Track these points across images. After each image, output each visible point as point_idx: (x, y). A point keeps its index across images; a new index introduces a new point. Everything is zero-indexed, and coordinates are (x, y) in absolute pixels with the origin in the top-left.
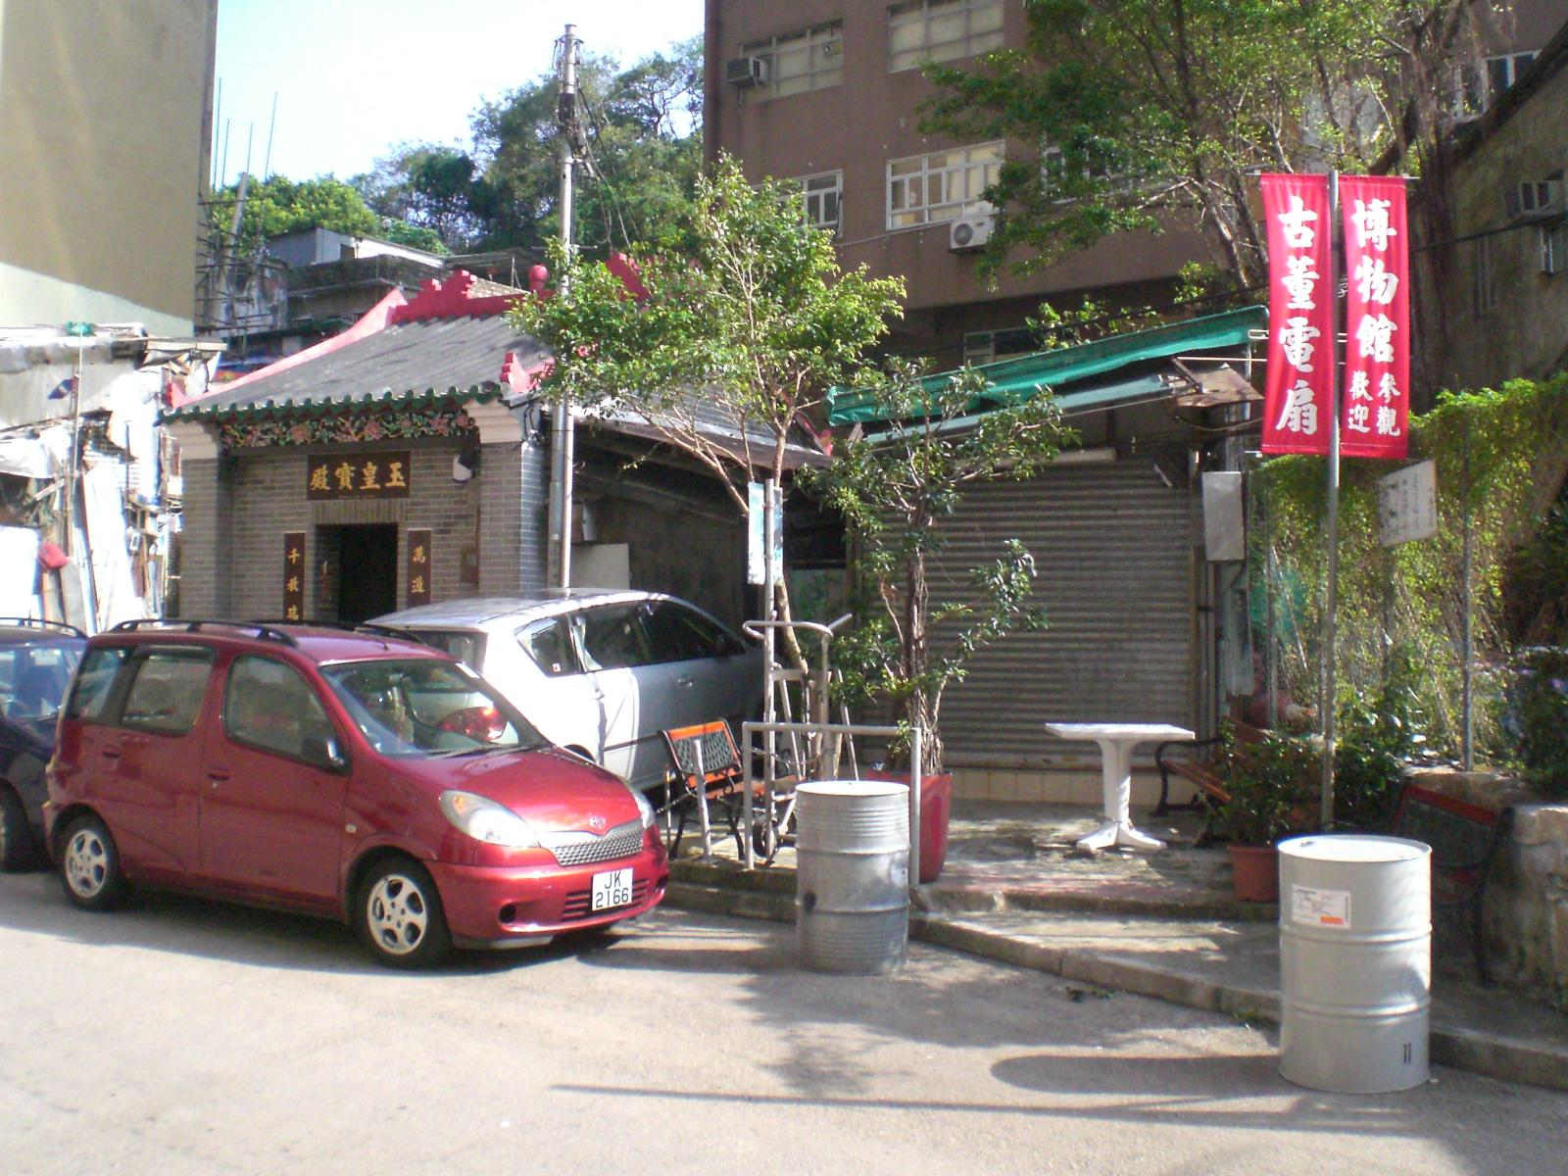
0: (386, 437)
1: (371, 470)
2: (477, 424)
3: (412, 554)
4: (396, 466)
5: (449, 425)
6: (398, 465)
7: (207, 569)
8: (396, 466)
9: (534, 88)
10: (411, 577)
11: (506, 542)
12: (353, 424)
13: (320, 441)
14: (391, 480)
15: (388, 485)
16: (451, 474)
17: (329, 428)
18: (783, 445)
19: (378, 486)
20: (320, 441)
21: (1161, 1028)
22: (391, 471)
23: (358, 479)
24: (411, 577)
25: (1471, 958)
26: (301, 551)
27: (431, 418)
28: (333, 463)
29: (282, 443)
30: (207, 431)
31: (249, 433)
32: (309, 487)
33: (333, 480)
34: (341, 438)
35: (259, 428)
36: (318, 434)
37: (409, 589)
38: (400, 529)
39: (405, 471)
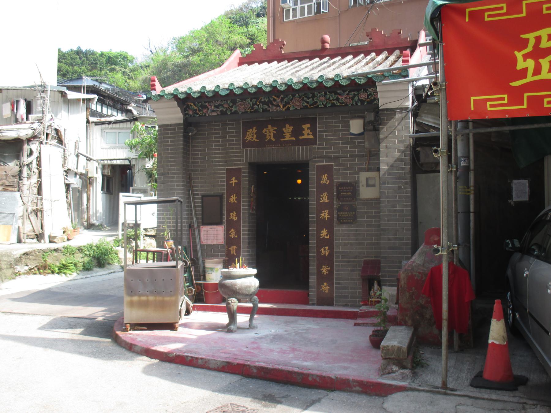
0: (306, 107)
1: (288, 130)
3: (319, 179)
4: (306, 126)
5: (353, 99)
6: (308, 125)
8: (306, 126)
10: (319, 193)
14: (303, 135)
15: (301, 138)
17: (264, 103)
18: (172, 225)
20: (257, 111)
22: (303, 130)
23: (279, 134)
24: (319, 193)
27: (340, 95)
28: (261, 125)
29: (229, 113)
30: (179, 106)
33: (261, 136)
38: (310, 164)
39: (313, 129)
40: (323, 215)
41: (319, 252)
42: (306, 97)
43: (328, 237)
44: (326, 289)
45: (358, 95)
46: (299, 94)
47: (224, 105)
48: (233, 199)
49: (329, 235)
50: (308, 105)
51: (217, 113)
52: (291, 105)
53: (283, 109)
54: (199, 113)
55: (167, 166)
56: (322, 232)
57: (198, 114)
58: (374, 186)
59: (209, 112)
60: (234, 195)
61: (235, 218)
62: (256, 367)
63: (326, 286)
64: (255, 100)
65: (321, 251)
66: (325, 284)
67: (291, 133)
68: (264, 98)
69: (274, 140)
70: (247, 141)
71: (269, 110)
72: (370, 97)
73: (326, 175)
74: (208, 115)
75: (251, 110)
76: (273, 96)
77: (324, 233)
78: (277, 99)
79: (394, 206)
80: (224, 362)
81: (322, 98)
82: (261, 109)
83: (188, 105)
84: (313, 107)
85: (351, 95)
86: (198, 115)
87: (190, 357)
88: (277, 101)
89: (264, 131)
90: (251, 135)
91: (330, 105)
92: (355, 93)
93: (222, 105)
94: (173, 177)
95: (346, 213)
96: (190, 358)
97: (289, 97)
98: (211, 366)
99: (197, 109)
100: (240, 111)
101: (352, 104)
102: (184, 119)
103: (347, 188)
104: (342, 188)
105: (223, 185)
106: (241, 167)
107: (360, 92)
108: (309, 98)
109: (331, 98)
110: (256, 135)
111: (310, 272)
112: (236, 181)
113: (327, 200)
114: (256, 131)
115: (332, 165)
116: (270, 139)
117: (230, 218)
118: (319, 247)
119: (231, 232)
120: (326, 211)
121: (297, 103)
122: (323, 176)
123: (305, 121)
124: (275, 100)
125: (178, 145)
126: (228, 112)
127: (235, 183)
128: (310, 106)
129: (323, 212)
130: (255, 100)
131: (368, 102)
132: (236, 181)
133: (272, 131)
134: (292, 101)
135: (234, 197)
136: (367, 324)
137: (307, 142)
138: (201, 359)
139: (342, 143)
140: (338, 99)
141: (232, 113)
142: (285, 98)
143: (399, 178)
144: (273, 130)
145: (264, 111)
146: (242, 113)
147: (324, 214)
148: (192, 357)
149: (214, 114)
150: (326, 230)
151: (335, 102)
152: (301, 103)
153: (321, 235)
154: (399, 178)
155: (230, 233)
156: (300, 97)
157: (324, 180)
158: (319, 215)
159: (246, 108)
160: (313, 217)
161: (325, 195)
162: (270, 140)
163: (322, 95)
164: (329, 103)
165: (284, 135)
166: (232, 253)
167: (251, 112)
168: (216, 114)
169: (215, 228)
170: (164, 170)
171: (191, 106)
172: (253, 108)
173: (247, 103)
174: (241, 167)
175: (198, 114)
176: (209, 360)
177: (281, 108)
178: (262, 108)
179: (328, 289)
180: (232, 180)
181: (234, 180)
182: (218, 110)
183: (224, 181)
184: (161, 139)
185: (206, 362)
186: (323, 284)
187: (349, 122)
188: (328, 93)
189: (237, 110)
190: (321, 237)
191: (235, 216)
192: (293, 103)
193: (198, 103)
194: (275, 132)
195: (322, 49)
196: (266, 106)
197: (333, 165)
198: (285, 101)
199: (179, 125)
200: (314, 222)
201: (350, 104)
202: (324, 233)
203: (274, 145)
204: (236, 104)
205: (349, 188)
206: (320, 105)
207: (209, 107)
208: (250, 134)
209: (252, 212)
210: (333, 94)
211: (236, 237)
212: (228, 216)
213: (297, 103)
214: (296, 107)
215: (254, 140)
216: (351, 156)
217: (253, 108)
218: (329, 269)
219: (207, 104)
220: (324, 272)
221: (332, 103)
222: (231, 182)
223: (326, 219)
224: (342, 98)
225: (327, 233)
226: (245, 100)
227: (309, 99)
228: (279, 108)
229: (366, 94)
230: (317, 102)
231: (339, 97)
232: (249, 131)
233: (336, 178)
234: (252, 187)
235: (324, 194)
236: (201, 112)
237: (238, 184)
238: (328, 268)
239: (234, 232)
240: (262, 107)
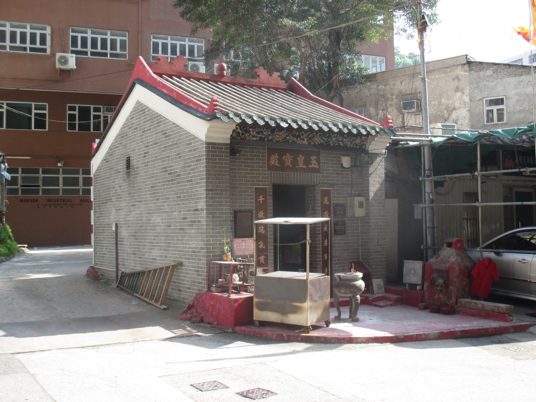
1: (301, 159)
3: (323, 200)
4: (313, 158)
6: (315, 157)
8: (313, 158)
13: (288, 141)
14: (312, 164)
15: (310, 166)
19: (305, 167)
20: (288, 141)
22: (312, 160)
23: (295, 162)
29: (266, 140)
32: (269, 164)
34: (299, 142)
39: (318, 161)
47: (264, 133)
55: (216, 182)
62: (459, 331)
67: (303, 162)
69: (291, 166)
73: (327, 197)
74: (248, 139)
79: (100, 209)
80: (439, 333)
85: (352, 139)
86: (240, 138)
87: (415, 335)
89: (284, 158)
93: (262, 132)
94: (221, 194)
95: (340, 227)
96: (415, 336)
97: (313, 134)
98: (431, 337)
99: (241, 132)
105: (253, 202)
106: (267, 187)
112: (264, 199)
114: (278, 157)
116: (288, 165)
125: (225, 164)
136: (388, 305)
138: (424, 334)
139: (337, 174)
140: (342, 141)
141: (268, 140)
142: (310, 134)
143: (380, 203)
144: (291, 158)
148: (417, 335)
149: (254, 139)
154: (380, 203)
165: (298, 163)
166: (261, 262)
167: (283, 142)
168: (256, 139)
169: (246, 240)
170: (212, 186)
174: (267, 187)
175: (240, 137)
176: (429, 334)
177: (305, 142)
180: (260, 198)
182: (258, 136)
183: (253, 199)
185: (427, 336)
194: (292, 160)
199: (226, 144)
211: (264, 248)
216: (342, 184)
227: (325, 138)
230: (330, 141)
232: (272, 156)
237: (265, 202)
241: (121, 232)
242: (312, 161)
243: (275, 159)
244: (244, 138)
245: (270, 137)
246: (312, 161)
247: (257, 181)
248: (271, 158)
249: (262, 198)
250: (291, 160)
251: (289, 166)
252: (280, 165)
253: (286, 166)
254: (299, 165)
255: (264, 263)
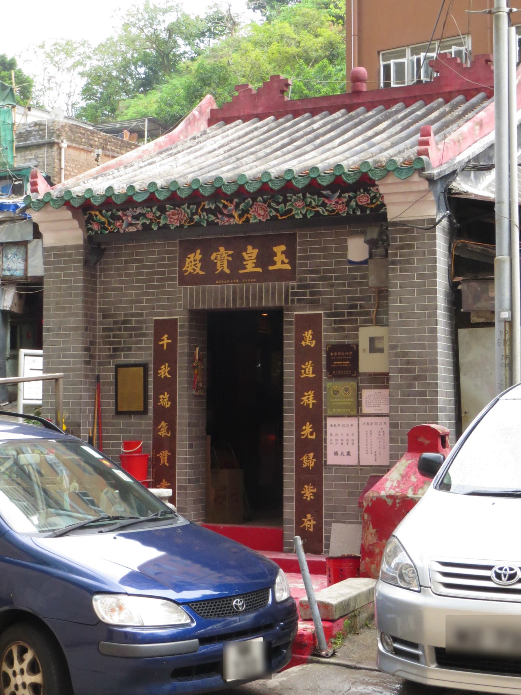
0: (274, 218)
2: (386, 201)
3: (300, 338)
4: (279, 249)
5: (348, 204)
6: (283, 248)
7: (74, 356)
8: (279, 249)
9: (6, 58)
10: (300, 362)
11: (75, 363)
12: (237, 207)
14: (274, 263)
15: (271, 268)
16: (345, 255)
17: (209, 211)
19: (259, 270)
20: (198, 224)
21: (177, 632)
22: (275, 254)
24: (300, 362)
25: (302, 580)
26: (173, 337)
27: (327, 197)
29: (155, 228)
31: (119, 218)
32: (181, 273)
35: (128, 213)
36: (196, 217)
37: (298, 373)
39: (290, 254)
40: (305, 399)
41: (299, 463)
42: (274, 202)
43: (313, 437)
44: (310, 525)
45: (355, 197)
46: (262, 197)
47: (147, 215)
48: (164, 371)
49: (314, 434)
50: (278, 215)
51: (136, 228)
52: (251, 215)
53: (239, 222)
54: (109, 228)
56: (304, 428)
57: (107, 229)
58: (381, 351)
59: (124, 227)
60: (165, 365)
61: (168, 404)
63: (310, 520)
64: (195, 206)
65: (303, 460)
66: (309, 516)
67: (255, 261)
68: (209, 204)
69: (228, 271)
70: (186, 274)
71: (217, 223)
72: (374, 201)
74: (122, 232)
75: (189, 223)
76: (222, 201)
77: (307, 429)
78: (229, 204)
81: (300, 203)
82: (206, 222)
83: (90, 214)
84: (285, 217)
85: (345, 197)
86: (107, 232)
88: (230, 208)
89: (213, 257)
90: (193, 263)
91: (312, 215)
92: (351, 194)
94: (67, 336)
97: (246, 201)
100: (173, 225)
101: (348, 213)
102: (86, 237)
103: (343, 354)
104: (336, 354)
107: (358, 193)
108: (278, 204)
109: (313, 204)
110: (200, 264)
111: (284, 496)
112: (170, 341)
113: (313, 374)
114: (201, 256)
115: (320, 315)
116: (222, 270)
117: (159, 404)
118: (299, 454)
119: (161, 428)
120: (310, 393)
121: (260, 212)
122: (306, 333)
123: (278, 240)
124: (225, 207)
125: (76, 282)
126: (153, 226)
127: (168, 344)
128: (281, 216)
129: (306, 394)
130: (195, 206)
131: (371, 209)
132: (170, 341)
133: (226, 258)
134: (252, 208)
135: (165, 367)
137: (281, 275)
141: (159, 228)
145: (210, 223)
146: (175, 228)
147: (307, 397)
150: (310, 424)
151: (320, 210)
152: (267, 211)
153: (303, 433)
155: (160, 429)
156: (265, 202)
157: (308, 339)
158: (298, 400)
159: (182, 219)
160: (290, 403)
161: (309, 366)
162: (222, 271)
163: (299, 197)
164: (311, 212)
165: (245, 263)
167: (189, 226)
168: (136, 230)
171: (96, 216)
172: (191, 220)
173: (183, 211)
175: (107, 229)
177: (237, 221)
178: (207, 220)
179: (314, 525)
180: (163, 340)
181: (166, 339)
182: (138, 224)
184: (50, 271)
186: (306, 517)
187: (346, 241)
188: (308, 195)
189: (168, 223)
190: (302, 437)
191: (167, 399)
192: (253, 212)
193: (107, 211)
194: (230, 259)
195: (352, 92)
196: (212, 216)
197: (321, 314)
198: (242, 209)
199: (77, 247)
200: (290, 411)
201: (344, 213)
202: (307, 429)
203: (228, 281)
204: (165, 214)
205: (347, 353)
206: (297, 214)
207: (124, 218)
208: (191, 262)
209: (197, 394)
210: (316, 197)
211: (169, 435)
212: (156, 400)
213: (261, 212)
214: (260, 218)
215: (198, 273)
217: (191, 220)
218: (315, 491)
219: (120, 213)
220: (307, 497)
221: (315, 211)
222: (161, 343)
223: (311, 407)
224: (331, 204)
225: (311, 430)
226: (179, 207)
228: (232, 220)
229: (367, 197)
230: (290, 211)
231: (326, 201)
232: (189, 256)
233: (326, 337)
234: (195, 350)
235: (307, 363)
236: (112, 227)
238: (313, 489)
239: (166, 428)
240: (206, 217)
241: (88, 390)
242: (276, 256)
243: (195, 261)
244: (115, 231)
245: (161, 221)
246: (276, 256)
247: (158, 307)
248: (188, 260)
249: (168, 339)
250: (228, 260)
251: (225, 272)
252: (204, 273)
253: (217, 272)
254: (246, 268)
255: (167, 465)
